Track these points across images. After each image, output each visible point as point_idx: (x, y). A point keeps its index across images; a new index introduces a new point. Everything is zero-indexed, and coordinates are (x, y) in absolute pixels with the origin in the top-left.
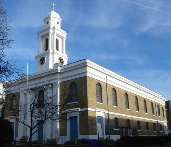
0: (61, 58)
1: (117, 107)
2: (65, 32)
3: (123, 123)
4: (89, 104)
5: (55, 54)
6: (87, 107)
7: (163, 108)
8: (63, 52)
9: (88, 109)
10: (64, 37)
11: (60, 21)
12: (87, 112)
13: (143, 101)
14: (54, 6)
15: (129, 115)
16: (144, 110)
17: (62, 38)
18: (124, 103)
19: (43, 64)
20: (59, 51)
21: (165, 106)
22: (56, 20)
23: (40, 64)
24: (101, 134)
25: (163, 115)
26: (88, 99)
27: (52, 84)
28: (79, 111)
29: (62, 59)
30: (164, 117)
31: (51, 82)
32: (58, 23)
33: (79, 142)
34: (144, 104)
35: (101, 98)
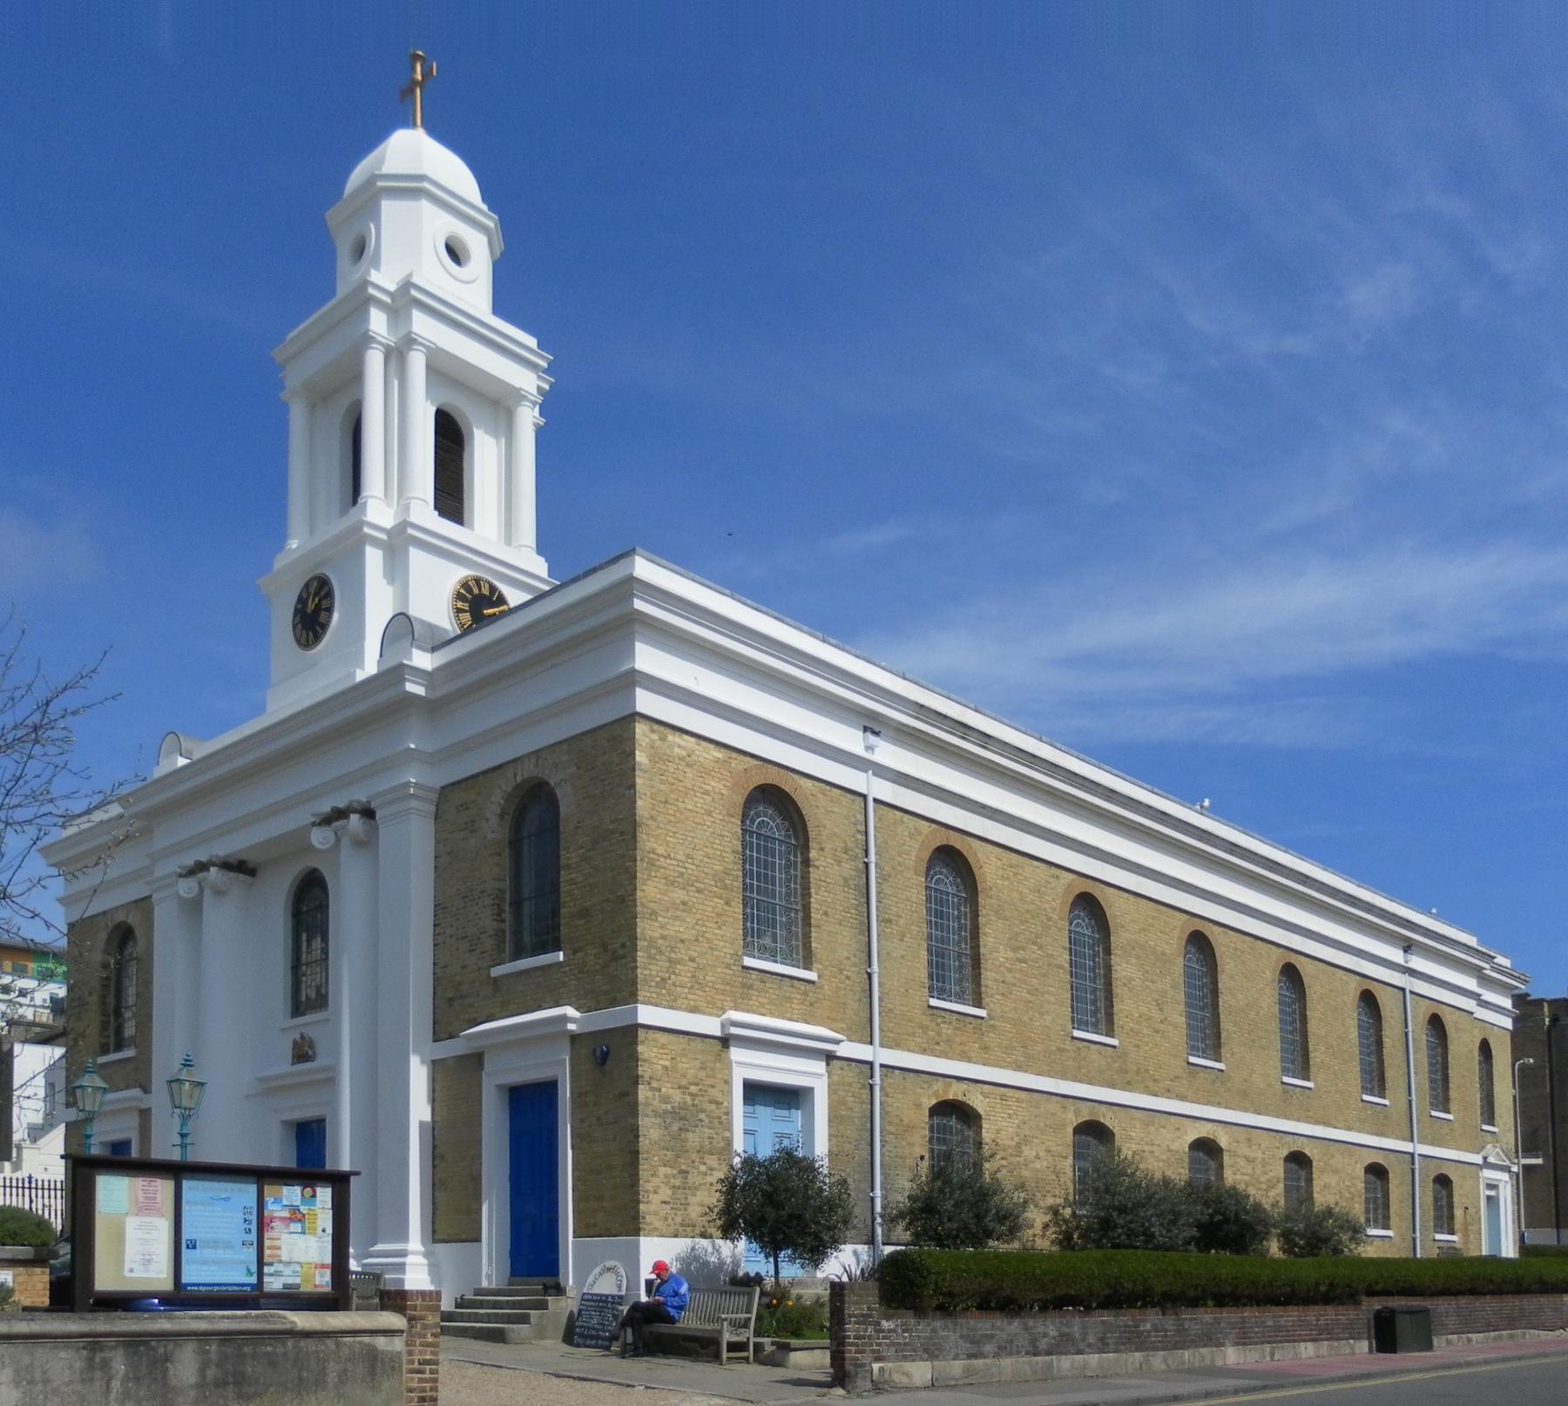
0: (477, 581)
1: (982, 1013)
2: (532, 342)
3: (1028, 1152)
4: (647, 967)
5: (414, 553)
6: (627, 992)
7: (1485, 1048)
8: (509, 536)
9: (635, 1012)
10: (517, 395)
11: (483, 239)
12: (634, 1042)
13: (1269, 973)
14: (427, 73)
15: (1112, 1085)
16: (1353, 1073)
17: (501, 404)
18: (1420, 1079)
19: (317, 638)
20: (471, 527)
21: (1514, 1034)
22: (438, 224)
23: (298, 641)
24: (381, 1319)
25: (1477, 1097)
26: (646, 929)
27: (368, 813)
28: (574, 1038)
29: (493, 589)
30: (1489, 1115)
31: (360, 795)
32: (455, 252)
33: (638, 1315)
34: (1431, 1048)
35: (1101, 1004)
